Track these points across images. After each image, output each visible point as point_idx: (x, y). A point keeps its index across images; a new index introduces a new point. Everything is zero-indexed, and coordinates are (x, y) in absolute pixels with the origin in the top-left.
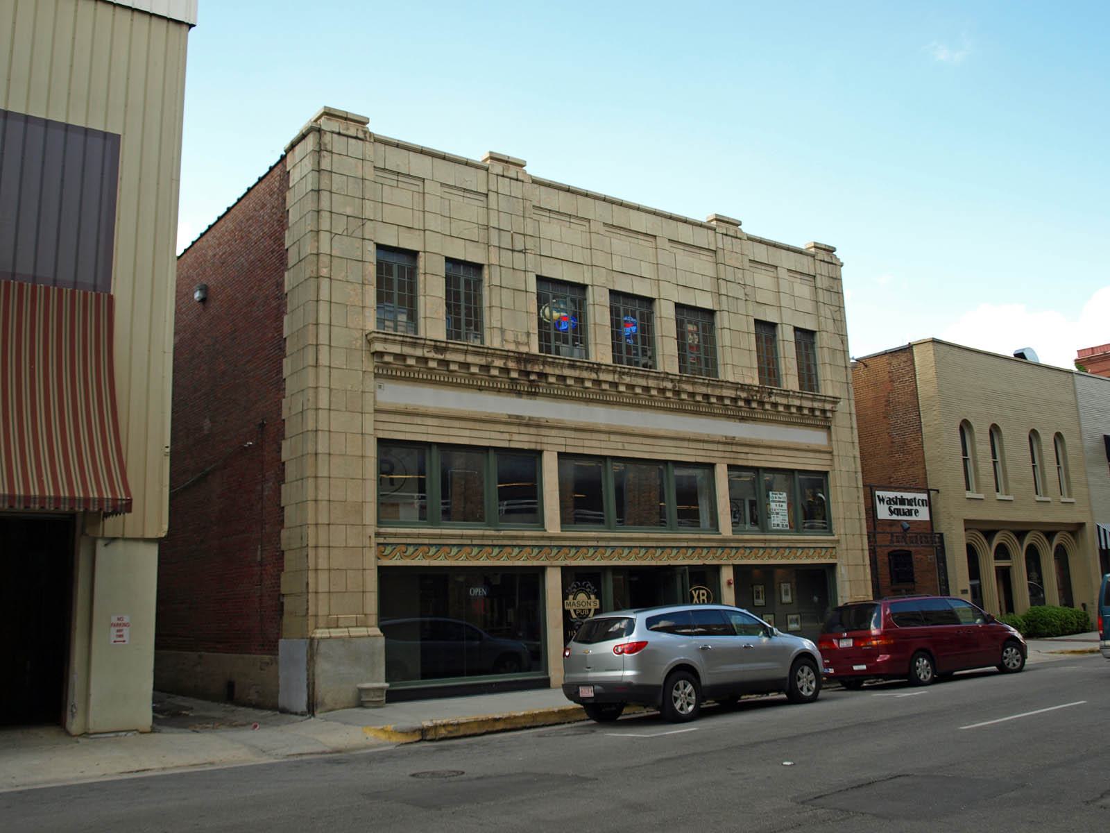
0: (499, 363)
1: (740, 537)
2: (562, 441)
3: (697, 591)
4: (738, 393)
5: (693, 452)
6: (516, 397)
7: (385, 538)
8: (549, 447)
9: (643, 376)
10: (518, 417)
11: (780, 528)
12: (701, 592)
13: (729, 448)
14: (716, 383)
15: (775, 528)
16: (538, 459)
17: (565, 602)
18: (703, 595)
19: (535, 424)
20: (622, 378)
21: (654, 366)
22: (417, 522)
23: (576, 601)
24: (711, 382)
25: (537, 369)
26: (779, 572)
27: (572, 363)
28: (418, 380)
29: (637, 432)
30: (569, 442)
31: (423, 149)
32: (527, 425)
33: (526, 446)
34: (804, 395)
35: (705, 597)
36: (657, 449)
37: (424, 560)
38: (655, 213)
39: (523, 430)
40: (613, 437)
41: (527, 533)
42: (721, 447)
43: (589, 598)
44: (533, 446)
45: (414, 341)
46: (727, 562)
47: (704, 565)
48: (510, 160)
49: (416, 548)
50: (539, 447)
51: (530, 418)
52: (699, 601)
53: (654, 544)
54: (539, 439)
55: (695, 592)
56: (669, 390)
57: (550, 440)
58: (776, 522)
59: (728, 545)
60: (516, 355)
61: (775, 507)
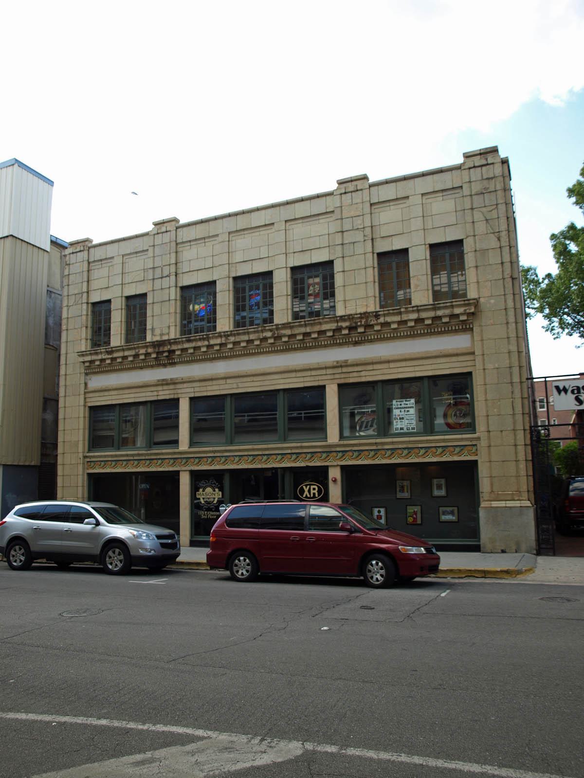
0: (142, 351)
1: (345, 442)
2: (192, 390)
3: (308, 487)
4: (340, 324)
5: (302, 379)
6: (163, 368)
7: (90, 458)
8: (183, 395)
9: (244, 334)
10: (163, 380)
11: (405, 430)
12: (312, 487)
13: (339, 370)
14: (312, 322)
15: (397, 431)
16: (469, 379)
17: (197, 493)
18: (314, 489)
19: (173, 382)
20: (228, 339)
21: (215, 328)
22: (446, 432)
23: (204, 493)
24: (307, 322)
25: (166, 349)
26: (400, 470)
27: (187, 339)
28: (459, 330)
29: (249, 373)
30: (197, 389)
31: (388, 180)
32: (167, 384)
33: (167, 397)
34: (454, 303)
35: (316, 491)
36: (209, 388)
37: (366, 460)
38: (273, 206)
39: (165, 387)
40: (229, 381)
41: (164, 451)
42: (329, 371)
43: (215, 491)
44: (172, 397)
45: (95, 351)
46: (184, 468)
47: (307, 466)
48: (164, 221)
49: (426, 450)
50: (176, 397)
51: (171, 379)
52: (310, 494)
53: (260, 453)
54: (175, 391)
55: (306, 487)
56: (270, 338)
57: (182, 391)
58: (399, 426)
59: (333, 449)
60: (151, 344)
61: (399, 413)
